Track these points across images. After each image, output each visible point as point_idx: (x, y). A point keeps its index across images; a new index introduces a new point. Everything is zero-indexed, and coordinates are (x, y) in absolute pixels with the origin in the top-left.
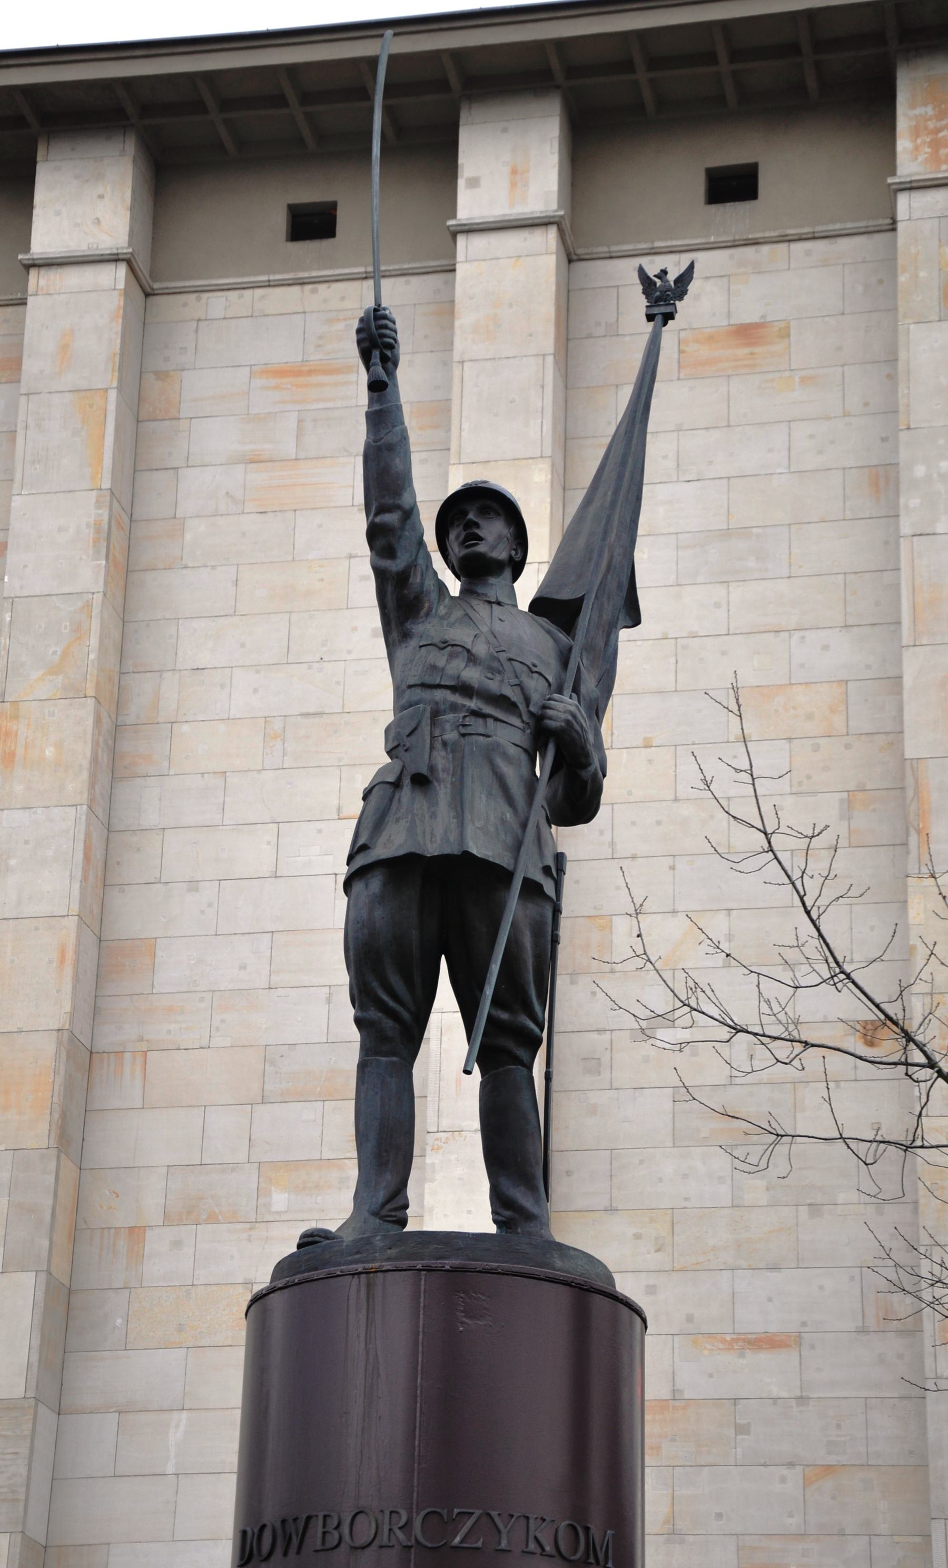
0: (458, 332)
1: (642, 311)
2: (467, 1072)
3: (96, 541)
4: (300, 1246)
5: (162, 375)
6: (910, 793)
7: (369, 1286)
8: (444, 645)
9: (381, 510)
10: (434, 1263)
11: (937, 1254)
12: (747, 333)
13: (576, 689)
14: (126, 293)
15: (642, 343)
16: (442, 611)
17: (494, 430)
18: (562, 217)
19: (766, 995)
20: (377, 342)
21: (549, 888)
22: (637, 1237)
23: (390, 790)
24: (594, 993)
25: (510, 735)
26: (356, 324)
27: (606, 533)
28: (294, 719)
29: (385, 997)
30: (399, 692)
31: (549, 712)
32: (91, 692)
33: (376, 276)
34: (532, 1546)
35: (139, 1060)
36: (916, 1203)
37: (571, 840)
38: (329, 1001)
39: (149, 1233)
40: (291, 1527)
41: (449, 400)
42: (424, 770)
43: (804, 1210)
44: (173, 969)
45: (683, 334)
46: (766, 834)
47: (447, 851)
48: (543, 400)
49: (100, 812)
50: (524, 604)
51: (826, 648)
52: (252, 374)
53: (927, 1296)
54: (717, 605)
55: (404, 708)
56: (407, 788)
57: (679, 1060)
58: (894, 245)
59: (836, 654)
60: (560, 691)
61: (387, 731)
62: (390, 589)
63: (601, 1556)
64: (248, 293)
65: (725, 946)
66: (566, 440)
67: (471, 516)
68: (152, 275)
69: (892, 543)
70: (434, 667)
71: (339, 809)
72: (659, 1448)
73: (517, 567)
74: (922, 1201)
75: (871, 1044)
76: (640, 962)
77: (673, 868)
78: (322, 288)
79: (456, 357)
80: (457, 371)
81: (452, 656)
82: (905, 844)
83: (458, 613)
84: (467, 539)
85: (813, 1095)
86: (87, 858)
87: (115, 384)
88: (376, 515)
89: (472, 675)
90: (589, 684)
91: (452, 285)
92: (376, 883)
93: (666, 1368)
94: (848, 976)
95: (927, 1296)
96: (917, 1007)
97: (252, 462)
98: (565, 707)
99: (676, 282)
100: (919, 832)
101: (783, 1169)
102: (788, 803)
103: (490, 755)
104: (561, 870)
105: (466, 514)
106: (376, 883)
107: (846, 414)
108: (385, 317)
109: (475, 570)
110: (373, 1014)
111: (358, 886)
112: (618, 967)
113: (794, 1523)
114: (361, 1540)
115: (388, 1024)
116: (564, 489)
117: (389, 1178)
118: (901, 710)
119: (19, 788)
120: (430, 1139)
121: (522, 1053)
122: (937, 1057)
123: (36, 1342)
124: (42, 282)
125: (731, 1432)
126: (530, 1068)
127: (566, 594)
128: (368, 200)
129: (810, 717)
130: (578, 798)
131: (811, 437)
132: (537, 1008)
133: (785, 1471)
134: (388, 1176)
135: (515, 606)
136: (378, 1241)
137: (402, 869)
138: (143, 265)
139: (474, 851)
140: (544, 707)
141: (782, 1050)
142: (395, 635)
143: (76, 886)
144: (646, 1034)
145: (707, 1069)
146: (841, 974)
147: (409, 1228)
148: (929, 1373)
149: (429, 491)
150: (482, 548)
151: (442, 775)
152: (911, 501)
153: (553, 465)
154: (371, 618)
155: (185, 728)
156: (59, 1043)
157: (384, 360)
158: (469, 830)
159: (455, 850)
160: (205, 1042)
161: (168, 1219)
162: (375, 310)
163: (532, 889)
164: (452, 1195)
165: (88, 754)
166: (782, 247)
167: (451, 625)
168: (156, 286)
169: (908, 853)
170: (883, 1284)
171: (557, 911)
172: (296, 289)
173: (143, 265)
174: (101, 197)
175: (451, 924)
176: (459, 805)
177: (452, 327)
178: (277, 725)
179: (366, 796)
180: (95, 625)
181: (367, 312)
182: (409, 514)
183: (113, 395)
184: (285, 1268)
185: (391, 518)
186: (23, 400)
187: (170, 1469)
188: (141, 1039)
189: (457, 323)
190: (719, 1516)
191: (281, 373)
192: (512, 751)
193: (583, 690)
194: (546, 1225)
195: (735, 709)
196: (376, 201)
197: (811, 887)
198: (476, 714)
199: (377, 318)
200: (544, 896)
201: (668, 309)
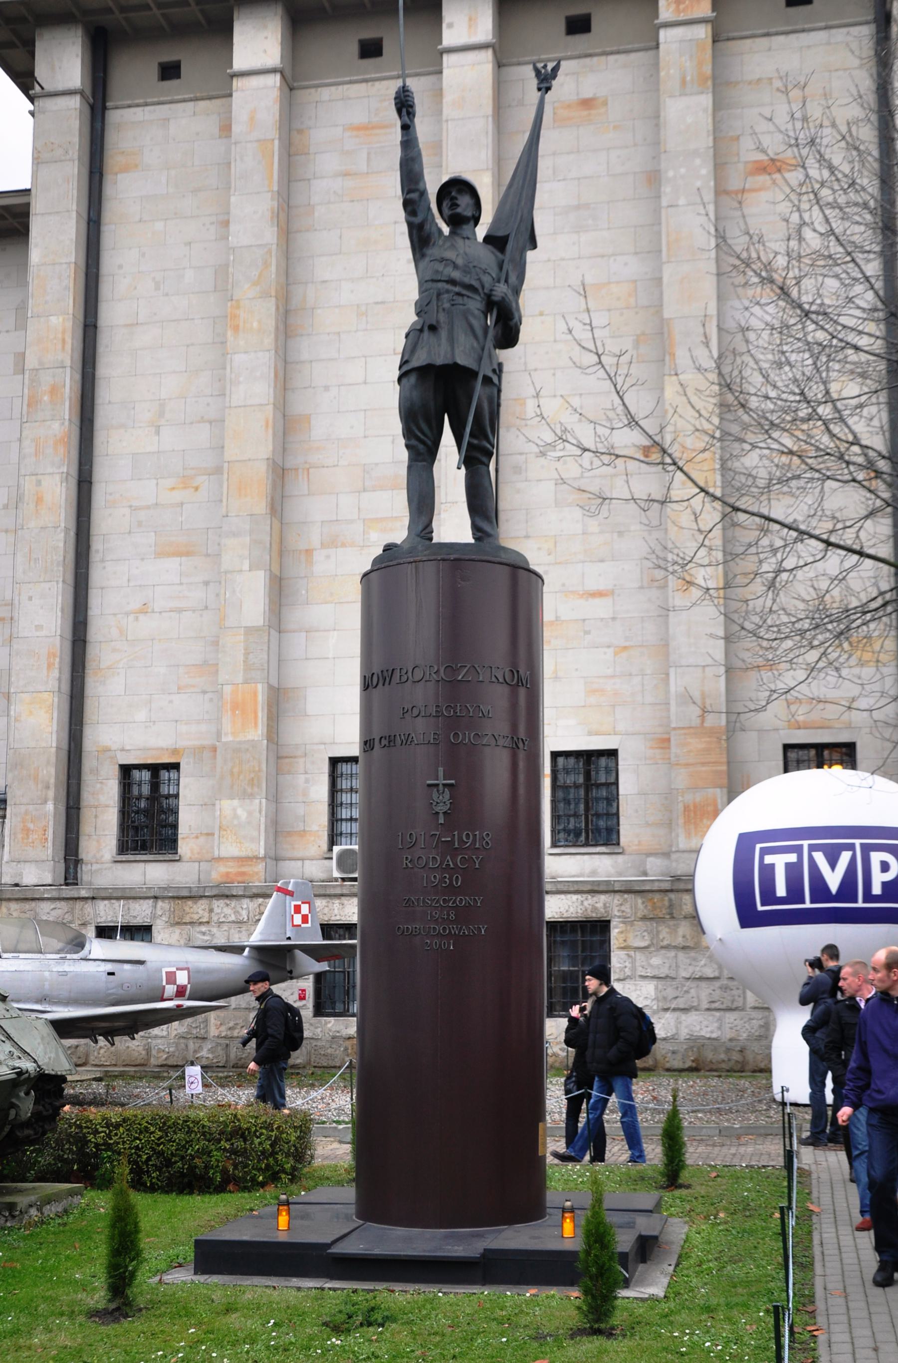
0: (444, 105)
2: (459, 468)
3: (272, 218)
4: (384, 551)
6: (666, 336)
7: (416, 568)
8: (442, 260)
9: (409, 192)
10: (446, 557)
11: (676, 551)
12: (587, 103)
13: (506, 281)
14: (281, 89)
15: (536, 101)
16: (441, 242)
17: (463, 149)
18: (495, 43)
19: (598, 433)
20: (404, 104)
21: (495, 379)
22: (539, 549)
23: (418, 333)
24: (517, 436)
25: (475, 304)
27: (519, 201)
28: (372, 297)
29: (419, 434)
31: (494, 293)
32: (273, 294)
33: (404, 76)
34: (494, 679)
35: (306, 473)
36: (666, 530)
37: (505, 355)
38: (393, 442)
39: (314, 552)
40: (385, 674)
41: (441, 141)
42: (434, 323)
43: (615, 535)
44: (319, 429)
46: (597, 354)
47: (446, 362)
48: (487, 140)
51: (626, 264)
52: (344, 130)
53: (671, 569)
54: (574, 244)
55: (423, 292)
56: (426, 333)
57: (559, 465)
58: (657, 57)
59: (630, 267)
60: (499, 281)
62: (415, 232)
63: (524, 683)
64: (340, 87)
65: (578, 410)
66: (499, 160)
67: (453, 194)
68: (293, 78)
69: (657, 212)
70: (437, 272)
71: (394, 350)
72: (550, 641)
73: (476, 220)
74: (669, 528)
75: (647, 456)
76: (539, 419)
77: (554, 375)
78: (377, 84)
79: (444, 118)
80: (444, 126)
81: (446, 266)
82: (664, 360)
83: (448, 244)
84: (451, 206)
85: (620, 482)
86: (276, 376)
87: (277, 136)
88: (407, 194)
89: (456, 275)
90: (513, 279)
91: (440, 80)
92: (413, 379)
93: (555, 607)
94: (637, 423)
95: (671, 569)
96: (668, 438)
97: (346, 175)
98: (501, 290)
99: (552, 70)
100: (670, 354)
101: (606, 515)
102: (608, 342)
103: (466, 314)
104: (501, 370)
105: (451, 193)
106: (413, 379)
107: (635, 145)
108: (408, 91)
109: (457, 221)
110: (414, 442)
111: (404, 381)
112: (529, 422)
113: (610, 672)
114: (417, 678)
115: (421, 447)
117: (424, 519)
118: (661, 294)
119: (242, 343)
120: (443, 506)
121: (484, 459)
122: (677, 460)
124: (239, 84)
125: (582, 634)
126: (488, 466)
127: (500, 233)
128: (397, 36)
129: (619, 299)
130: (508, 335)
131: (619, 157)
133: (606, 650)
134: (423, 518)
135: (476, 239)
136: (420, 548)
138: (288, 73)
139: (459, 362)
141: (606, 459)
142: (418, 256)
143: (272, 390)
144: (543, 454)
145: (571, 470)
146: (633, 422)
147: (434, 541)
148: (671, 604)
150: (459, 210)
151: (443, 325)
152: (667, 189)
155: (319, 311)
156: (268, 465)
157: (409, 113)
158: (457, 352)
159: (450, 362)
160: (336, 463)
161: (323, 546)
162: (403, 87)
163: (487, 380)
164: (453, 525)
166: (603, 58)
167: (445, 250)
168: (295, 84)
169: (664, 365)
170: (651, 565)
171: (499, 391)
172: (364, 85)
173: (288, 73)
174: (266, 38)
175: (450, 399)
176: (451, 340)
177: (441, 102)
178: (363, 309)
179: (407, 336)
181: (399, 88)
182: (423, 193)
183: (276, 142)
184: (376, 561)
185: (414, 196)
186: (233, 147)
187: (331, 656)
188: (306, 463)
189: (444, 101)
190: (577, 670)
191: (358, 128)
192: (476, 312)
193: (510, 281)
194: (496, 537)
195: (582, 292)
196: (402, 29)
197: (620, 380)
198: (458, 294)
199: (404, 91)
200: (493, 382)
201: (548, 85)
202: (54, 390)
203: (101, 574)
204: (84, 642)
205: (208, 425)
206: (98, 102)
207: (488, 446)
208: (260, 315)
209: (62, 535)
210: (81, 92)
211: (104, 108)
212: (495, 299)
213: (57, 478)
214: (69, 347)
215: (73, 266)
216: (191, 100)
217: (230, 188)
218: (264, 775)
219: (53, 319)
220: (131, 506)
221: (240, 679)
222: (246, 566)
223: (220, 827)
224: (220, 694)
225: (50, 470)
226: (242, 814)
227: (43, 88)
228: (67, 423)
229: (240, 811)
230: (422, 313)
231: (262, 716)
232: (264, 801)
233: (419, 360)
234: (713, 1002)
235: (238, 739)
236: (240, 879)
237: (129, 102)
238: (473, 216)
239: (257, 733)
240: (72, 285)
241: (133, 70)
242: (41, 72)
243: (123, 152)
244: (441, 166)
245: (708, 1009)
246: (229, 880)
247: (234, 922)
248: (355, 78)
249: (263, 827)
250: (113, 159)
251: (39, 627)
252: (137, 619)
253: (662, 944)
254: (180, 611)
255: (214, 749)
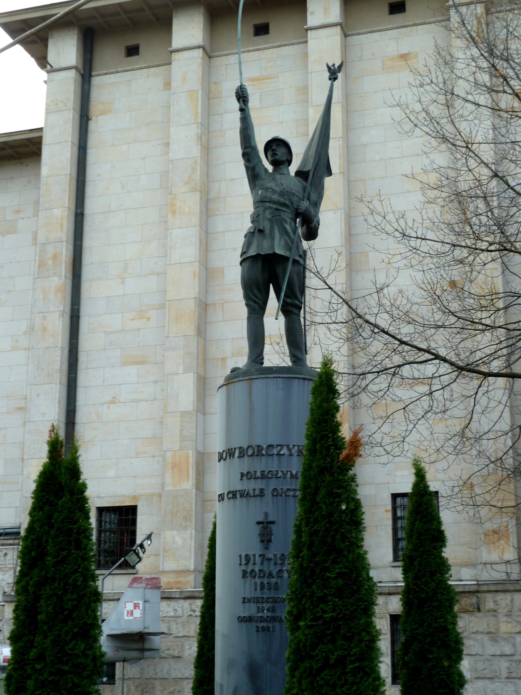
1: (328, 77)
4: (231, 372)
5: (216, 83)
13: (309, 199)
14: (203, 58)
21: (301, 261)
25: (287, 216)
26: (235, 91)
30: (255, 203)
32: (198, 189)
42: (262, 228)
45: (383, 58)
49: (204, 228)
50: (292, 174)
54: (398, 148)
61: (251, 216)
62: (250, 172)
67: (274, 147)
68: (209, 53)
73: (290, 162)
79: (309, 71)
80: (310, 76)
86: (200, 243)
87: (200, 88)
89: (275, 197)
90: (314, 197)
91: (307, 47)
98: (305, 204)
105: (272, 147)
108: (243, 88)
109: (276, 163)
110: (251, 303)
111: (243, 264)
115: (256, 306)
116: (347, 112)
121: (295, 311)
123: (195, 394)
130: (312, 234)
132: (300, 298)
135: (289, 174)
137: (255, 258)
138: (208, 50)
139: (278, 251)
140: (298, 206)
149: (261, 139)
153: (342, 105)
154: (246, 181)
163: (295, 262)
164: (276, 355)
165: (199, 209)
166: (415, 27)
172: (257, 52)
174: (193, 28)
177: (307, 61)
180: (198, 167)
181: (238, 87)
182: (254, 149)
183: (200, 92)
185: (247, 150)
189: (309, 60)
192: (288, 220)
193: (311, 199)
202: (55, 257)
203: (84, 378)
204: (73, 423)
205: (156, 276)
206: (86, 73)
207: (297, 302)
208: (191, 203)
209: (59, 352)
210: (76, 68)
211: (90, 76)
212: (301, 211)
213: (57, 314)
214: (65, 229)
215: (68, 176)
216: (146, 68)
217: (170, 122)
218: (193, 513)
219: (56, 211)
220: (105, 332)
221: (177, 448)
222: (181, 370)
223: (164, 550)
224: (164, 457)
225: (52, 309)
226: (179, 540)
227: (52, 67)
228: (63, 278)
229: (177, 539)
230: (255, 222)
231: (192, 472)
232: (193, 531)
233: (252, 252)
234: (511, 673)
235: (176, 489)
236: (177, 586)
237: (106, 71)
238: (287, 160)
239: (189, 484)
240: (67, 188)
241: (109, 53)
242: (51, 57)
243: (102, 103)
244: (308, 102)
245: (507, 678)
246: (170, 587)
247: (173, 617)
248: (252, 48)
249: (193, 549)
250: (95, 107)
251: (44, 414)
252: (109, 407)
253: (472, 631)
254: (138, 401)
255: (160, 496)
